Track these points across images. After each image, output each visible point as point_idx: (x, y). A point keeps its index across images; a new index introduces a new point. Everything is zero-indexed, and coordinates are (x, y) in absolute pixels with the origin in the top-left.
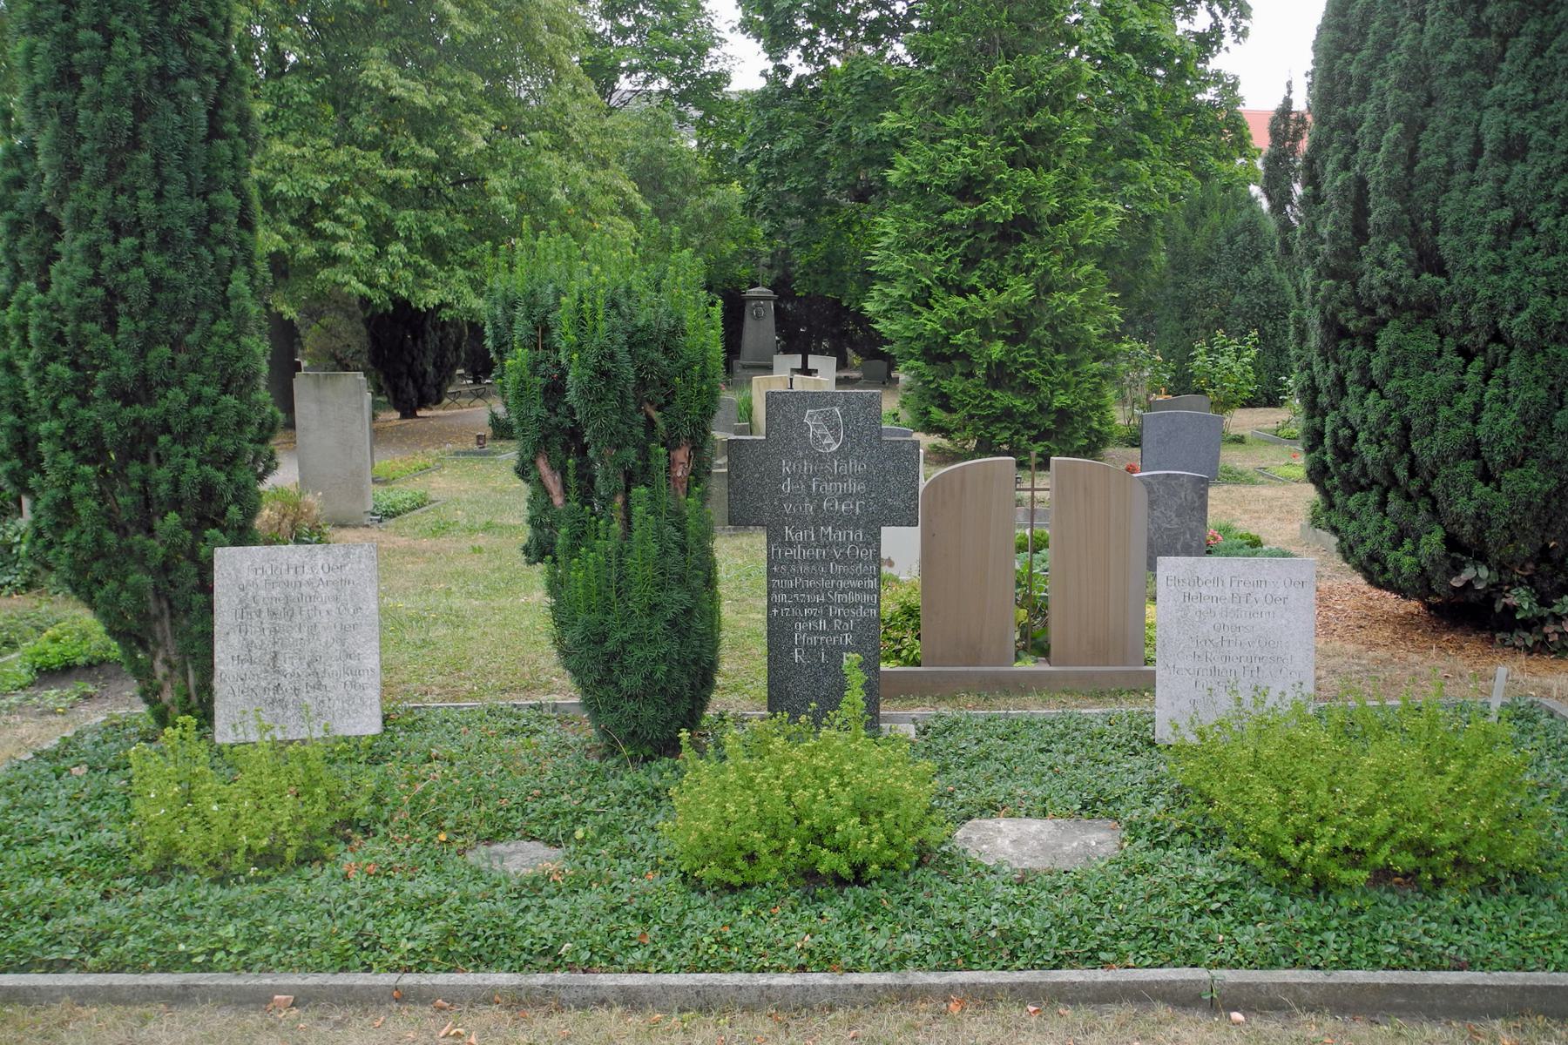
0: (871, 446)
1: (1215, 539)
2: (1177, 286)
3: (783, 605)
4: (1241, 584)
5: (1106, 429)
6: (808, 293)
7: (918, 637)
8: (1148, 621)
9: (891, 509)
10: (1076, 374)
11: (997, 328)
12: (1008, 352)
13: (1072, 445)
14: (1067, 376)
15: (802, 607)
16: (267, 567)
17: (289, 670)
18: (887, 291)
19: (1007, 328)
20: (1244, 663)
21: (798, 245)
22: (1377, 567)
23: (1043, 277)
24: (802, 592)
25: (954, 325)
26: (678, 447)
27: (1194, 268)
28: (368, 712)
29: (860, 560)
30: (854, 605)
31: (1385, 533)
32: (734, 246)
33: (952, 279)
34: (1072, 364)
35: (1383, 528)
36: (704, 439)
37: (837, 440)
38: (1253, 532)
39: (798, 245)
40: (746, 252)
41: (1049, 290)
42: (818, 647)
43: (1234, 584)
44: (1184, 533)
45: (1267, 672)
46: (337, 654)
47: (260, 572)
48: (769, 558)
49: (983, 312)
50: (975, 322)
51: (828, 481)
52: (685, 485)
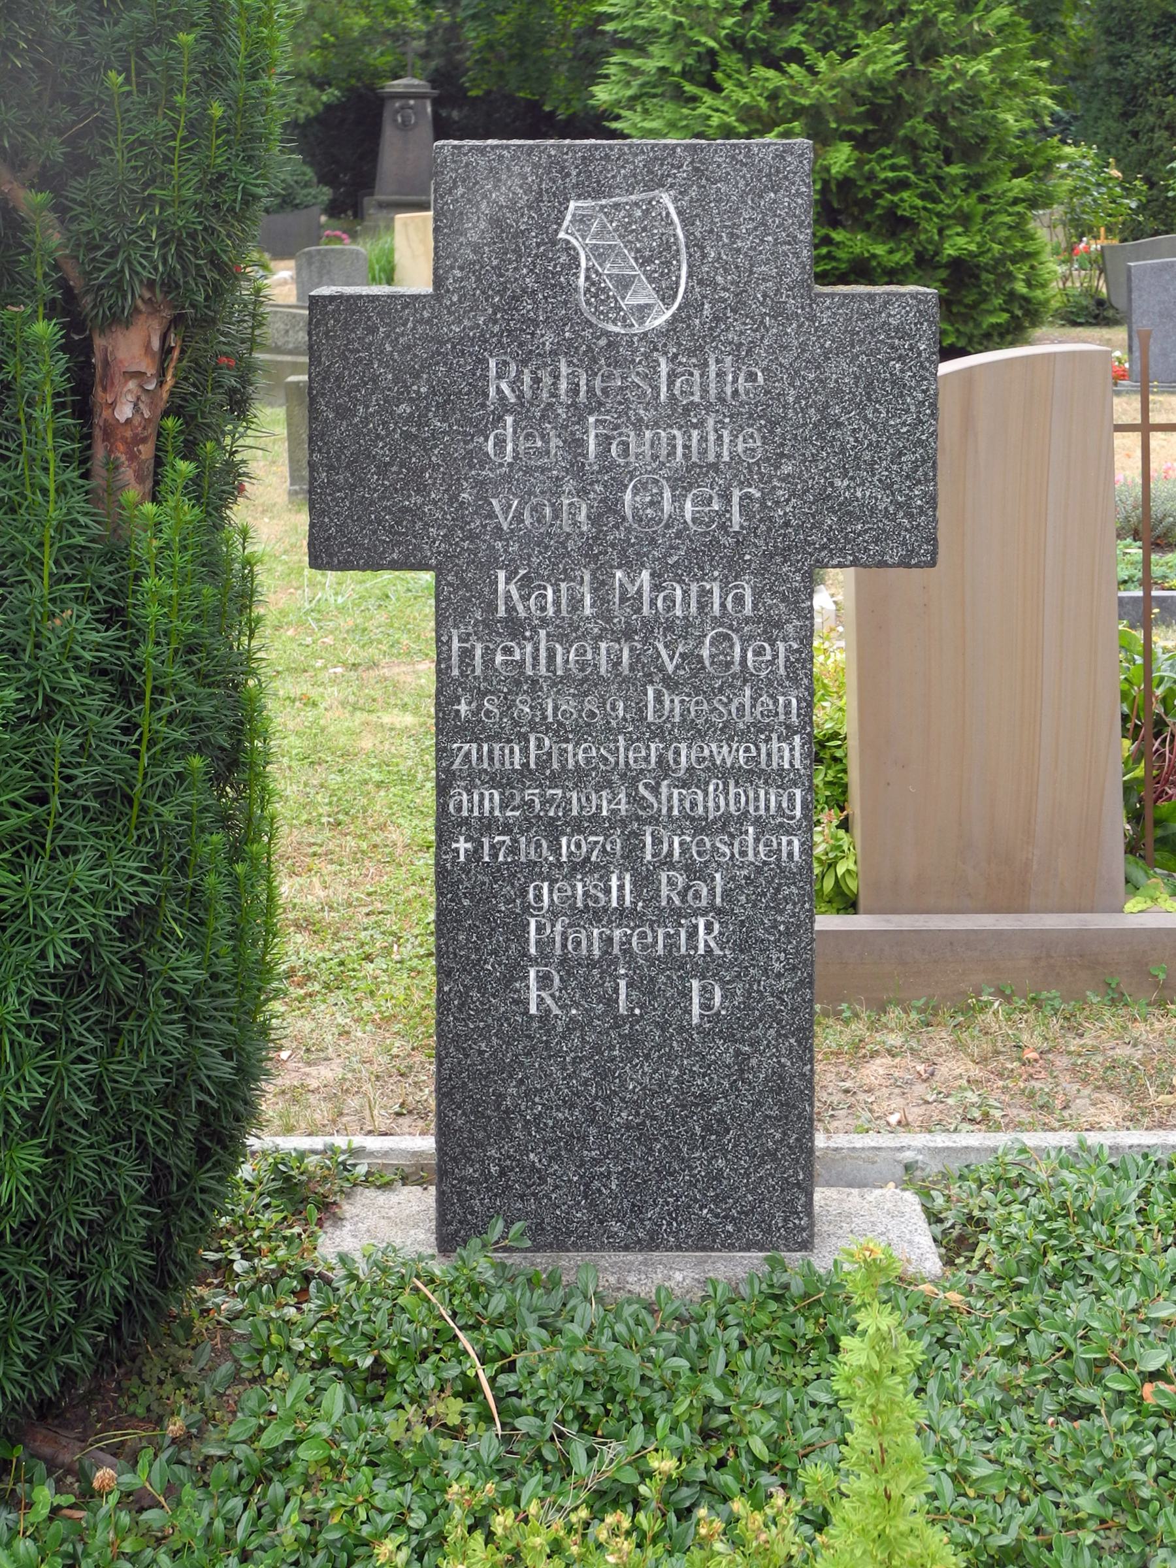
0: (778, 312)
2: (1115, 62)
3: (488, 825)
5: (1038, 293)
6: (488, 92)
7: (845, 825)
9: (847, 512)
10: (983, 199)
11: (837, 121)
12: (860, 163)
13: (978, 325)
14: (968, 203)
15: (553, 830)
18: (636, 62)
19: (854, 120)
21: (474, 17)
23: (919, 31)
24: (555, 780)
25: (759, 119)
26: (118, 319)
27: (1145, 30)
29: (746, 676)
30: (728, 825)
32: (365, 21)
33: (754, 38)
34: (975, 182)
36: (217, 293)
37: (667, 297)
39: (474, 17)
40: (388, 33)
41: (931, 54)
42: (607, 963)
48: (442, 673)
49: (815, 93)
50: (798, 112)
51: (639, 425)
52: (146, 451)
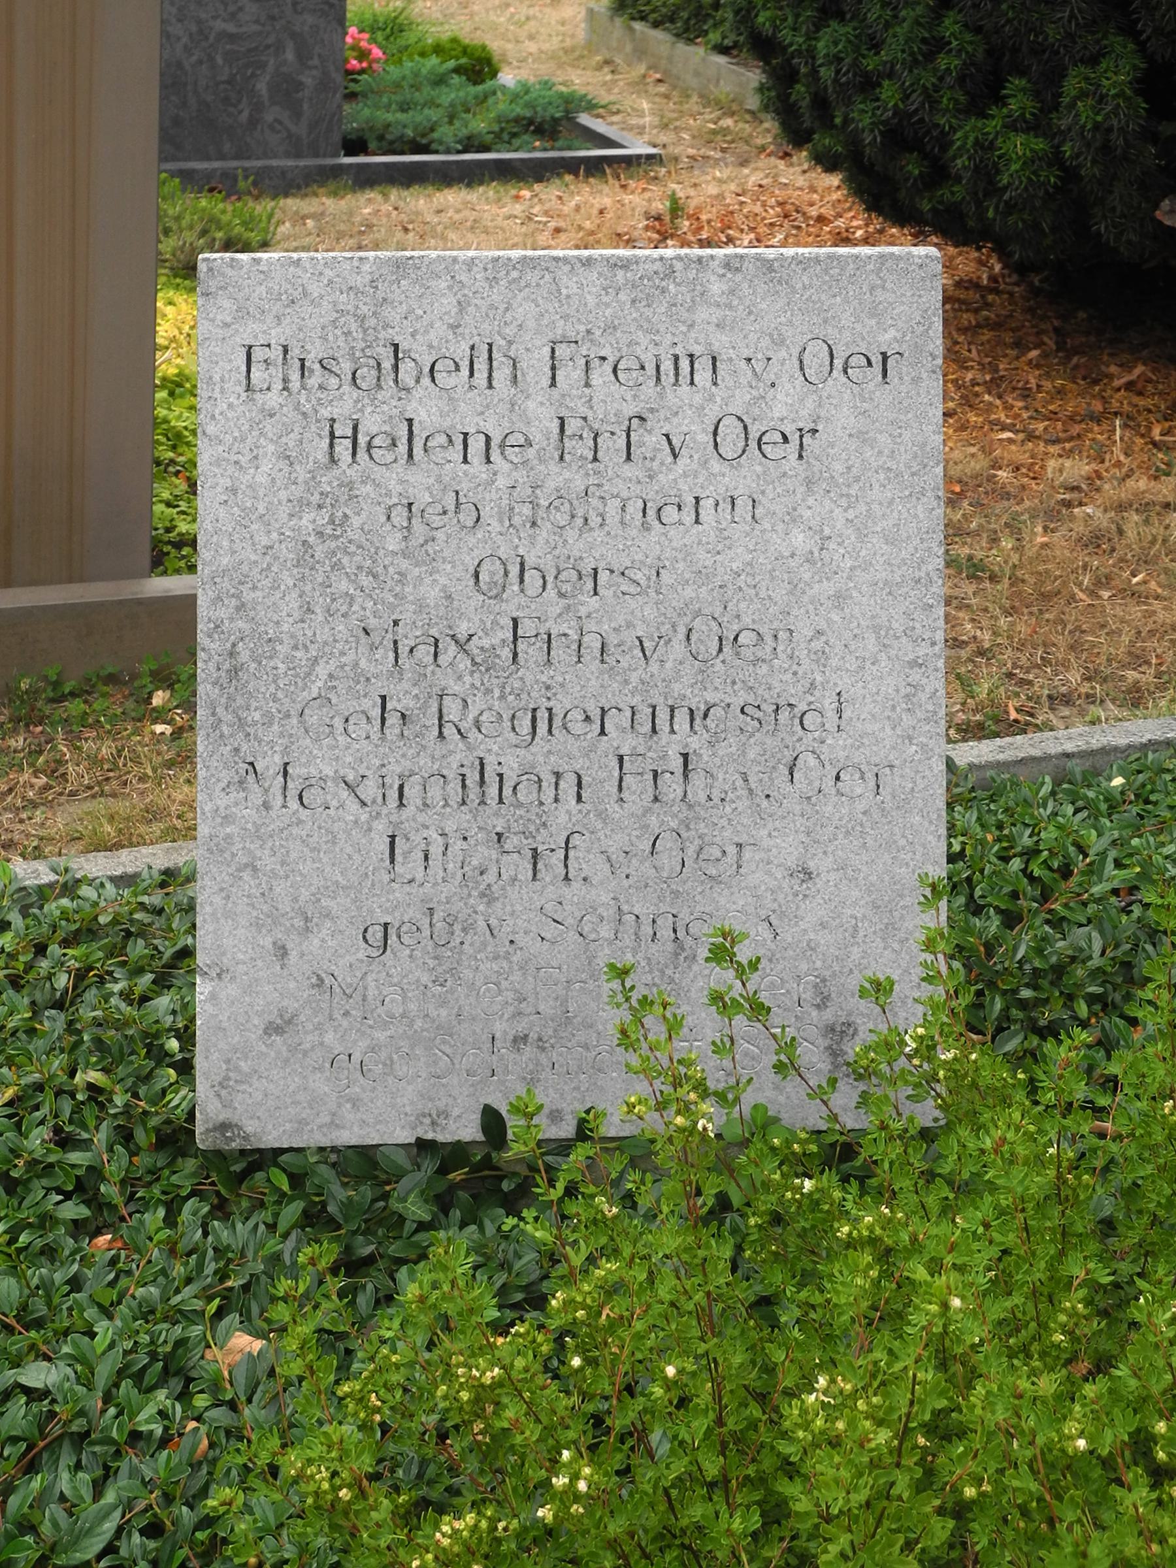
1: (363, 55)
4: (601, 375)
8: (167, 365)
20: (620, 739)
22: (913, 167)
31: (943, 62)
35: (937, 45)
38: (468, 36)
43: (569, 375)
44: (279, 48)
45: (727, 778)
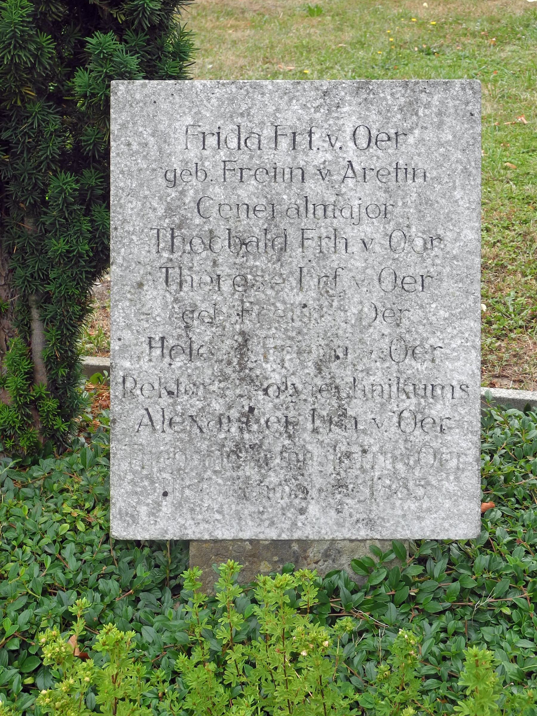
16: (226, 132)
17: (276, 378)
28: (450, 486)
46: (384, 344)
47: (212, 141)
